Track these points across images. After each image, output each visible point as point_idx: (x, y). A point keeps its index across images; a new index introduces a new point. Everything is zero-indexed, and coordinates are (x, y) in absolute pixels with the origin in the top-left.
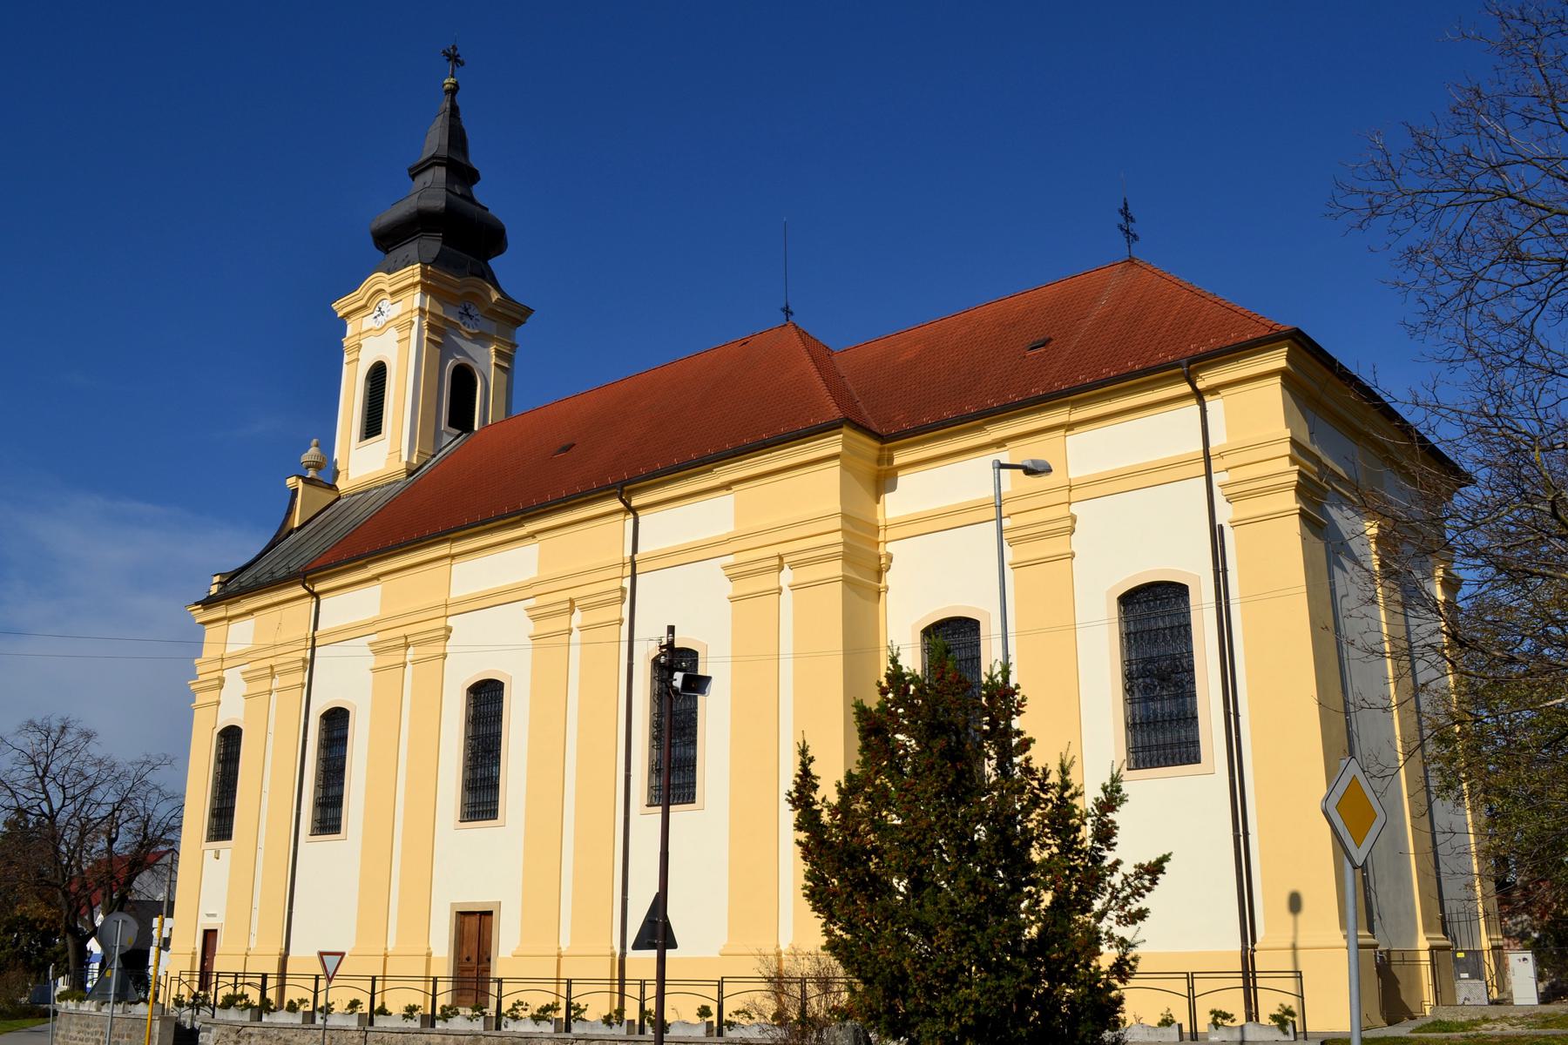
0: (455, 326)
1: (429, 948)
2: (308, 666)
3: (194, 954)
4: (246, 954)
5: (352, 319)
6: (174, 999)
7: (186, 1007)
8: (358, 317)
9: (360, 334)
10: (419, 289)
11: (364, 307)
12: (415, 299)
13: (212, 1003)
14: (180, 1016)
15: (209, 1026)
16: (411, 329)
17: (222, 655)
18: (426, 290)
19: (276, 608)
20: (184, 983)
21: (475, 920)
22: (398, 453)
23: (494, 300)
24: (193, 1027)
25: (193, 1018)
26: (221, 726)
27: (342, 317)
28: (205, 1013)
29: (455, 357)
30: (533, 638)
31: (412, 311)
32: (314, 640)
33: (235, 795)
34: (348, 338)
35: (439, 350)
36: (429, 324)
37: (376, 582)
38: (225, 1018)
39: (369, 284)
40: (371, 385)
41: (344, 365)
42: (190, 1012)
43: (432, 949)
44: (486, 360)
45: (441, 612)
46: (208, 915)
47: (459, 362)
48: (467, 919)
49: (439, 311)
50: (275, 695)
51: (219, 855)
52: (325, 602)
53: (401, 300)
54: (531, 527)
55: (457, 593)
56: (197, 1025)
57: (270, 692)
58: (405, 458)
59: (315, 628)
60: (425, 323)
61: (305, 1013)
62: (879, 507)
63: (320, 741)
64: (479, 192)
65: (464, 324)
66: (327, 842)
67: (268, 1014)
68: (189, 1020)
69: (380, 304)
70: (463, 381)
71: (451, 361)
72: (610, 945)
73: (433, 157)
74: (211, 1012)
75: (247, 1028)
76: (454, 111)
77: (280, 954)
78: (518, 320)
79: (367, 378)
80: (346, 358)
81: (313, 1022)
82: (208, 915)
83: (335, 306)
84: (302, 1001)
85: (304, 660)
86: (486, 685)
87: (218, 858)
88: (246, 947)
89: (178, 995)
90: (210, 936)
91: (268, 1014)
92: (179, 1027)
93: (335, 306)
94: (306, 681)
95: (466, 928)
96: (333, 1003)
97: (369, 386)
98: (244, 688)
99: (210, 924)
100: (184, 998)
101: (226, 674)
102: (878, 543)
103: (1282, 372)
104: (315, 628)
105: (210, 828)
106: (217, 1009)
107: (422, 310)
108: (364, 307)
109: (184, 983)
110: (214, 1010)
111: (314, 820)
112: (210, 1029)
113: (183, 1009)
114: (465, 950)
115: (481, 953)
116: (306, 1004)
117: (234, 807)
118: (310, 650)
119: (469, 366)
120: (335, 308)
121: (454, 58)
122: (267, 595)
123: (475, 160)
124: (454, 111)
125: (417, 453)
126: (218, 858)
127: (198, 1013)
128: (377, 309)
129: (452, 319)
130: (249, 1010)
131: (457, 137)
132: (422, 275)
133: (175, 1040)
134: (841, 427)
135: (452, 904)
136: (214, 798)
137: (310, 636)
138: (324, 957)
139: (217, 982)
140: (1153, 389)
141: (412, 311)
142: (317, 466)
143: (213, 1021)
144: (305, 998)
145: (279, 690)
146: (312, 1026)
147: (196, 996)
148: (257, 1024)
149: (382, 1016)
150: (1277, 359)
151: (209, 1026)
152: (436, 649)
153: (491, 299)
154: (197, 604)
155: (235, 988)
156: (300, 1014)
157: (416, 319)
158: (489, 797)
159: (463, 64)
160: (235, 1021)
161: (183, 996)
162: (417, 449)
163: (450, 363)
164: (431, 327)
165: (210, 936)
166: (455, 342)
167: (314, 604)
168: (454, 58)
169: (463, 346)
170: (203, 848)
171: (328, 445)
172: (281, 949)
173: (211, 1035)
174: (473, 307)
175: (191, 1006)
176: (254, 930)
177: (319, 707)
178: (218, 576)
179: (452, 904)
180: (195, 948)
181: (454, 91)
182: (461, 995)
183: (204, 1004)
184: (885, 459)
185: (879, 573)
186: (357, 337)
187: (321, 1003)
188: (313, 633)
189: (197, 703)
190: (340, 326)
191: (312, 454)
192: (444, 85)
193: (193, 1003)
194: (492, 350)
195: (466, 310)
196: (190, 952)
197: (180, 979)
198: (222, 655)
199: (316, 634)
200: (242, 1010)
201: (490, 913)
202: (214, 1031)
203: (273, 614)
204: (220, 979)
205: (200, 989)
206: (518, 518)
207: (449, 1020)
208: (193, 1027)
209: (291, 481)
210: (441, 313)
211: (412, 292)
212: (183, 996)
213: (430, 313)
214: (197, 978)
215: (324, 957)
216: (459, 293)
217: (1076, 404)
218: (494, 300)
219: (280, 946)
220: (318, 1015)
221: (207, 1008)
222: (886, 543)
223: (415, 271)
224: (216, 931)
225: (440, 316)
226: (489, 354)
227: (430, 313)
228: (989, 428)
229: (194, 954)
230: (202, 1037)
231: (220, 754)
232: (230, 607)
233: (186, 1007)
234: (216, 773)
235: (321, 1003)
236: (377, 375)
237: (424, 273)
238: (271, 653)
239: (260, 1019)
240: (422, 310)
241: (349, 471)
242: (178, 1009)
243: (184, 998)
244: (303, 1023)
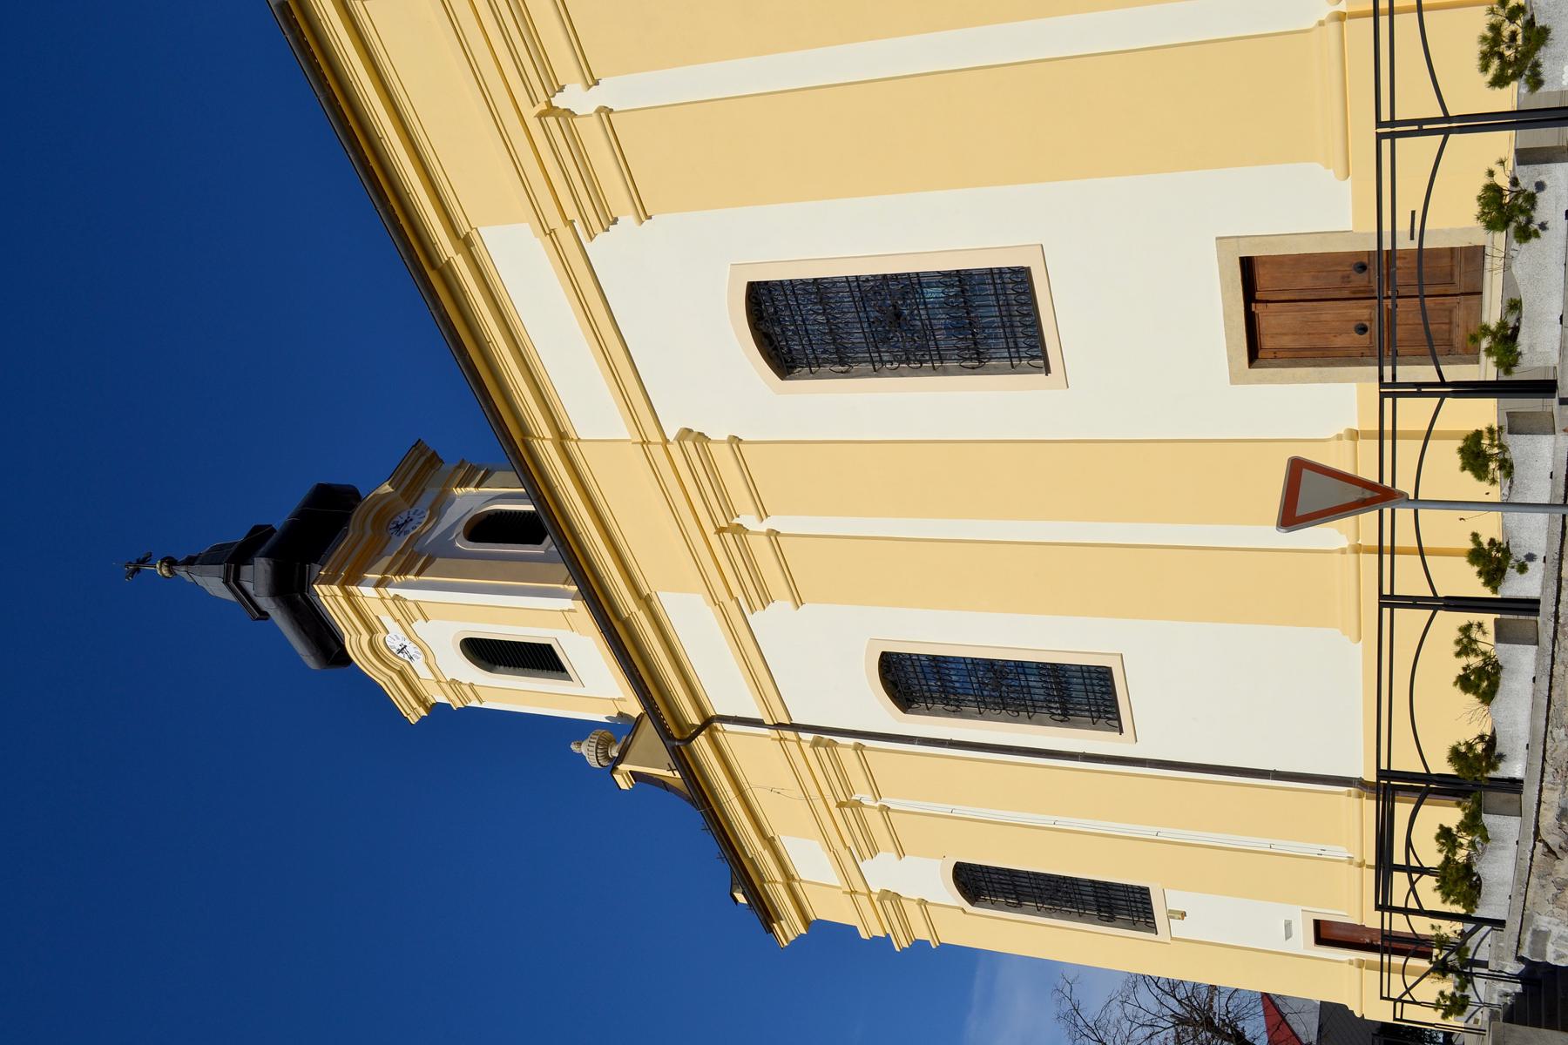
0: (414, 539)
1: (1339, 437)
2: (826, 737)
5: (426, 694)
6: (1444, 1016)
7: (1469, 991)
8: (419, 684)
9: (439, 682)
10: (353, 589)
11: (401, 674)
12: (366, 593)
13: (1459, 926)
14: (1489, 1005)
15: (1527, 938)
16: (405, 599)
17: (844, 892)
18: (355, 578)
19: (749, 793)
20: (1408, 991)
21: (1269, 318)
22: (565, 613)
23: (391, 490)
24: (1517, 976)
25: (1497, 976)
26: (955, 898)
27: (426, 708)
28: (1485, 947)
29: (454, 539)
30: (644, 215)
31: (382, 599)
32: (779, 726)
33: (1105, 884)
34: (449, 699)
35: (437, 559)
37: (656, 604)
38: (1508, 890)
39: (365, 664)
40: (500, 665)
41: (484, 706)
42: (1480, 983)
44: (470, 499)
45: (657, 452)
46: (1288, 936)
47: (462, 534)
48: (1266, 342)
49: (386, 561)
50: (886, 801)
51: (1177, 912)
52: (718, 707)
53: (377, 617)
54: (446, 247)
55: (621, 429)
56: (1513, 968)
57: (885, 809)
58: (568, 604)
59: (758, 723)
60: (397, 579)
61: (1500, 637)
63: (948, 714)
65: (414, 528)
66: (1132, 694)
67: (1501, 757)
68: (1501, 986)
69: (395, 651)
70: (489, 528)
71: (458, 545)
73: (226, 582)
74: (1486, 928)
75: (1543, 823)
77: (1360, 796)
78: (429, 460)
79: (490, 671)
80: (475, 703)
81: (1530, 606)
82: (1288, 936)
83: (414, 719)
84: (1466, 645)
85: (815, 744)
86: (767, 336)
87: (1184, 914)
88: (1345, 865)
89: (1437, 1006)
90: (1326, 934)
91: (1501, 757)
92: (1514, 1013)
93: (414, 719)
94: (851, 741)
95: (1287, 342)
96: (1475, 536)
97: (502, 667)
98: (887, 856)
99: (1305, 933)
100: (1448, 993)
101: (876, 889)
104: (758, 723)
105: (1133, 925)
106: (1479, 913)
107: (378, 584)
108: (401, 674)
109: (1408, 991)
110: (1482, 922)
111: (1094, 725)
112: (1536, 933)
113: (1473, 998)
114: (1339, 342)
115: (1346, 294)
116: (1475, 634)
117: (1093, 882)
118: (801, 735)
119: (469, 522)
120: (417, 720)
122: (727, 807)
125: (566, 586)
126: (1184, 914)
127: (1485, 964)
128: (401, 655)
130: (1487, 819)
131: (210, 558)
132: (331, 583)
133: (1551, 1026)
135: (1235, 379)
136: (1081, 917)
137: (774, 733)
139: (1406, 911)
141: (382, 599)
142: (604, 745)
143: (1513, 926)
144: (1457, 635)
145: (877, 794)
146: (1547, 608)
147: (1442, 969)
148: (1530, 793)
149: (1523, 340)
151: (1527, 938)
152: (723, 457)
153: (390, 493)
154: (771, 930)
155: (1423, 871)
156: (1502, 652)
157: (392, 591)
158: (993, 309)
160: (1518, 859)
161: (1442, 993)
162: (561, 586)
163: (463, 545)
164: (403, 571)
165: (1326, 934)
166: (435, 539)
167: (727, 727)
169: (444, 529)
170: (1169, 941)
171: (581, 729)
172: (1349, 794)
173: (1556, 931)
174: (398, 519)
175: (1466, 979)
176: (1312, 849)
177: (883, 714)
178: (735, 894)
179: (1235, 379)
180: (1351, 962)
181: (171, 562)
182: (1450, 344)
183: (1459, 948)
186: (444, 685)
187: (1472, 584)
188: (769, 727)
189: (927, 937)
190: (438, 711)
191: (587, 750)
192: (163, 575)
193: (1459, 973)
194: (458, 491)
197: (1400, 999)
198: (844, 892)
199: (768, 721)
200: (1486, 839)
201: (1248, 266)
202: (1543, 922)
203: (760, 799)
204: (1398, 902)
205: (1426, 955)
206: (433, 277)
207: (1539, 23)
208: (1519, 977)
209: (623, 783)
210: (391, 558)
211: (360, 599)
212: (1442, 993)
213: (385, 572)
214: (1398, 960)
215: (1300, 512)
216: (369, 532)
218: (391, 490)
219: (1344, 797)
220: (1517, 586)
221: (1472, 943)
223: (326, 593)
224: (1317, 923)
225: (393, 560)
226: (464, 496)
227: (385, 572)
230: (1560, 956)
231: (1007, 903)
232: (767, 876)
233: (1469, 991)
234: (1038, 911)
235: (1472, 584)
236: (486, 653)
237: (329, 581)
238: (819, 804)
239: (1514, 785)
240: (379, 584)
241: (616, 697)
242: (1470, 1009)
243: (1448, 993)
244: (1537, 643)
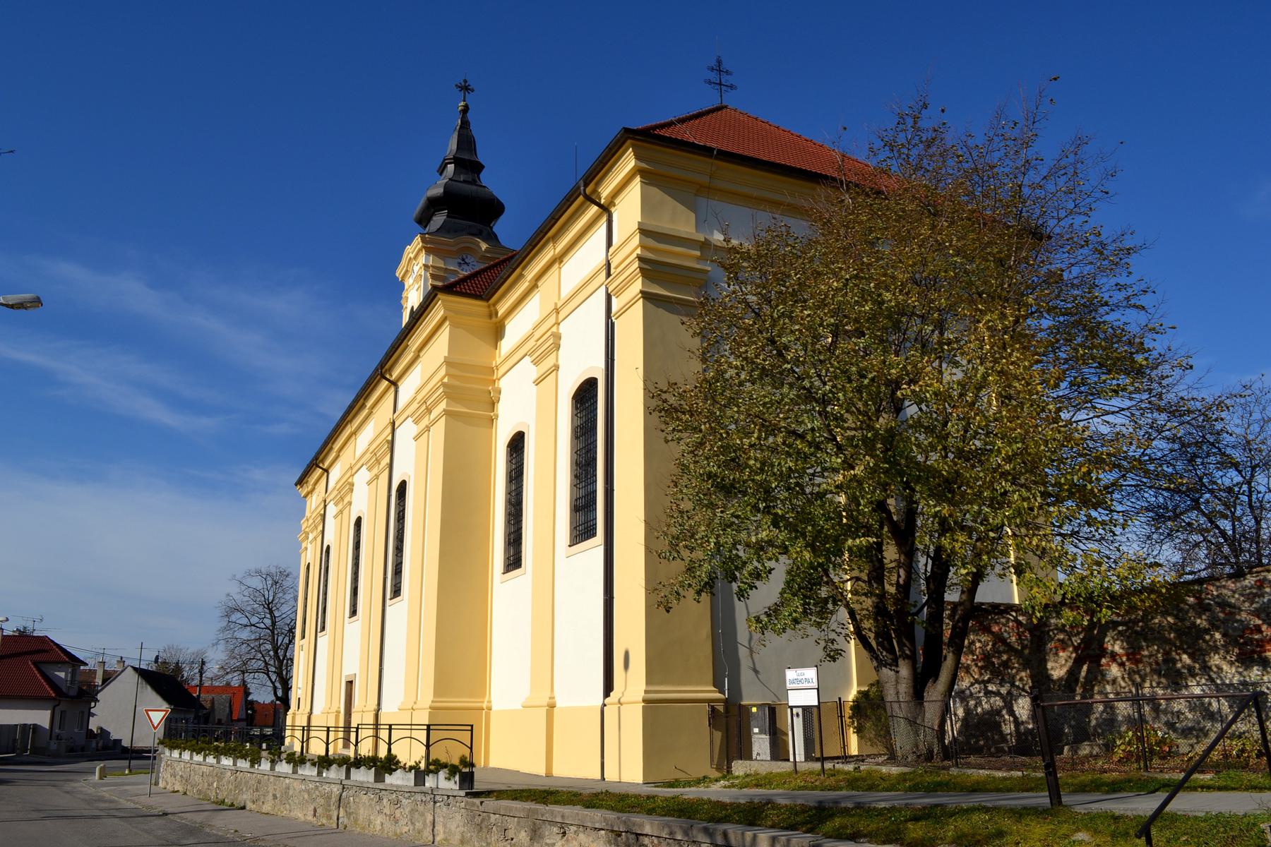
3: (338, 712)
4: (619, 702)
18: (429, 251)
23: (483, 249)
36: (431, 275)
43: (557, 699)
49: (441, 264)
62: (497, 351)
64: (486, 178)
72: (414, 700)
76: (465, 124)
102: (495, 381)
103: (637, 171)
121: (465, 88)
123: (482, 157)
124: (465, 124)
129: (452, 268)
134: (436, 295)
138: (149, 713)
140: (583, 213)
150: (628, 162)
159: (473, 91)
168: (465, 88)
174: (469, 257)
184: (493, 314)
185: (493, 404)
195: (463, 260)
196: (428, 706)
206: (362, 401)
210: (443, 266)
215: (149, 713)
216: (454, 249)
217: (555, 238)
222: (499, 380)
228: (525, 273)
229: (338, 712)
237: (423, 240)
240: (426, 266)
